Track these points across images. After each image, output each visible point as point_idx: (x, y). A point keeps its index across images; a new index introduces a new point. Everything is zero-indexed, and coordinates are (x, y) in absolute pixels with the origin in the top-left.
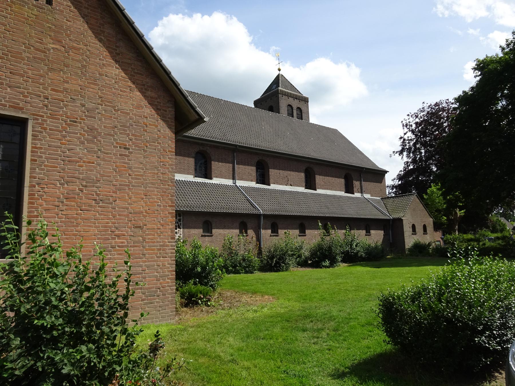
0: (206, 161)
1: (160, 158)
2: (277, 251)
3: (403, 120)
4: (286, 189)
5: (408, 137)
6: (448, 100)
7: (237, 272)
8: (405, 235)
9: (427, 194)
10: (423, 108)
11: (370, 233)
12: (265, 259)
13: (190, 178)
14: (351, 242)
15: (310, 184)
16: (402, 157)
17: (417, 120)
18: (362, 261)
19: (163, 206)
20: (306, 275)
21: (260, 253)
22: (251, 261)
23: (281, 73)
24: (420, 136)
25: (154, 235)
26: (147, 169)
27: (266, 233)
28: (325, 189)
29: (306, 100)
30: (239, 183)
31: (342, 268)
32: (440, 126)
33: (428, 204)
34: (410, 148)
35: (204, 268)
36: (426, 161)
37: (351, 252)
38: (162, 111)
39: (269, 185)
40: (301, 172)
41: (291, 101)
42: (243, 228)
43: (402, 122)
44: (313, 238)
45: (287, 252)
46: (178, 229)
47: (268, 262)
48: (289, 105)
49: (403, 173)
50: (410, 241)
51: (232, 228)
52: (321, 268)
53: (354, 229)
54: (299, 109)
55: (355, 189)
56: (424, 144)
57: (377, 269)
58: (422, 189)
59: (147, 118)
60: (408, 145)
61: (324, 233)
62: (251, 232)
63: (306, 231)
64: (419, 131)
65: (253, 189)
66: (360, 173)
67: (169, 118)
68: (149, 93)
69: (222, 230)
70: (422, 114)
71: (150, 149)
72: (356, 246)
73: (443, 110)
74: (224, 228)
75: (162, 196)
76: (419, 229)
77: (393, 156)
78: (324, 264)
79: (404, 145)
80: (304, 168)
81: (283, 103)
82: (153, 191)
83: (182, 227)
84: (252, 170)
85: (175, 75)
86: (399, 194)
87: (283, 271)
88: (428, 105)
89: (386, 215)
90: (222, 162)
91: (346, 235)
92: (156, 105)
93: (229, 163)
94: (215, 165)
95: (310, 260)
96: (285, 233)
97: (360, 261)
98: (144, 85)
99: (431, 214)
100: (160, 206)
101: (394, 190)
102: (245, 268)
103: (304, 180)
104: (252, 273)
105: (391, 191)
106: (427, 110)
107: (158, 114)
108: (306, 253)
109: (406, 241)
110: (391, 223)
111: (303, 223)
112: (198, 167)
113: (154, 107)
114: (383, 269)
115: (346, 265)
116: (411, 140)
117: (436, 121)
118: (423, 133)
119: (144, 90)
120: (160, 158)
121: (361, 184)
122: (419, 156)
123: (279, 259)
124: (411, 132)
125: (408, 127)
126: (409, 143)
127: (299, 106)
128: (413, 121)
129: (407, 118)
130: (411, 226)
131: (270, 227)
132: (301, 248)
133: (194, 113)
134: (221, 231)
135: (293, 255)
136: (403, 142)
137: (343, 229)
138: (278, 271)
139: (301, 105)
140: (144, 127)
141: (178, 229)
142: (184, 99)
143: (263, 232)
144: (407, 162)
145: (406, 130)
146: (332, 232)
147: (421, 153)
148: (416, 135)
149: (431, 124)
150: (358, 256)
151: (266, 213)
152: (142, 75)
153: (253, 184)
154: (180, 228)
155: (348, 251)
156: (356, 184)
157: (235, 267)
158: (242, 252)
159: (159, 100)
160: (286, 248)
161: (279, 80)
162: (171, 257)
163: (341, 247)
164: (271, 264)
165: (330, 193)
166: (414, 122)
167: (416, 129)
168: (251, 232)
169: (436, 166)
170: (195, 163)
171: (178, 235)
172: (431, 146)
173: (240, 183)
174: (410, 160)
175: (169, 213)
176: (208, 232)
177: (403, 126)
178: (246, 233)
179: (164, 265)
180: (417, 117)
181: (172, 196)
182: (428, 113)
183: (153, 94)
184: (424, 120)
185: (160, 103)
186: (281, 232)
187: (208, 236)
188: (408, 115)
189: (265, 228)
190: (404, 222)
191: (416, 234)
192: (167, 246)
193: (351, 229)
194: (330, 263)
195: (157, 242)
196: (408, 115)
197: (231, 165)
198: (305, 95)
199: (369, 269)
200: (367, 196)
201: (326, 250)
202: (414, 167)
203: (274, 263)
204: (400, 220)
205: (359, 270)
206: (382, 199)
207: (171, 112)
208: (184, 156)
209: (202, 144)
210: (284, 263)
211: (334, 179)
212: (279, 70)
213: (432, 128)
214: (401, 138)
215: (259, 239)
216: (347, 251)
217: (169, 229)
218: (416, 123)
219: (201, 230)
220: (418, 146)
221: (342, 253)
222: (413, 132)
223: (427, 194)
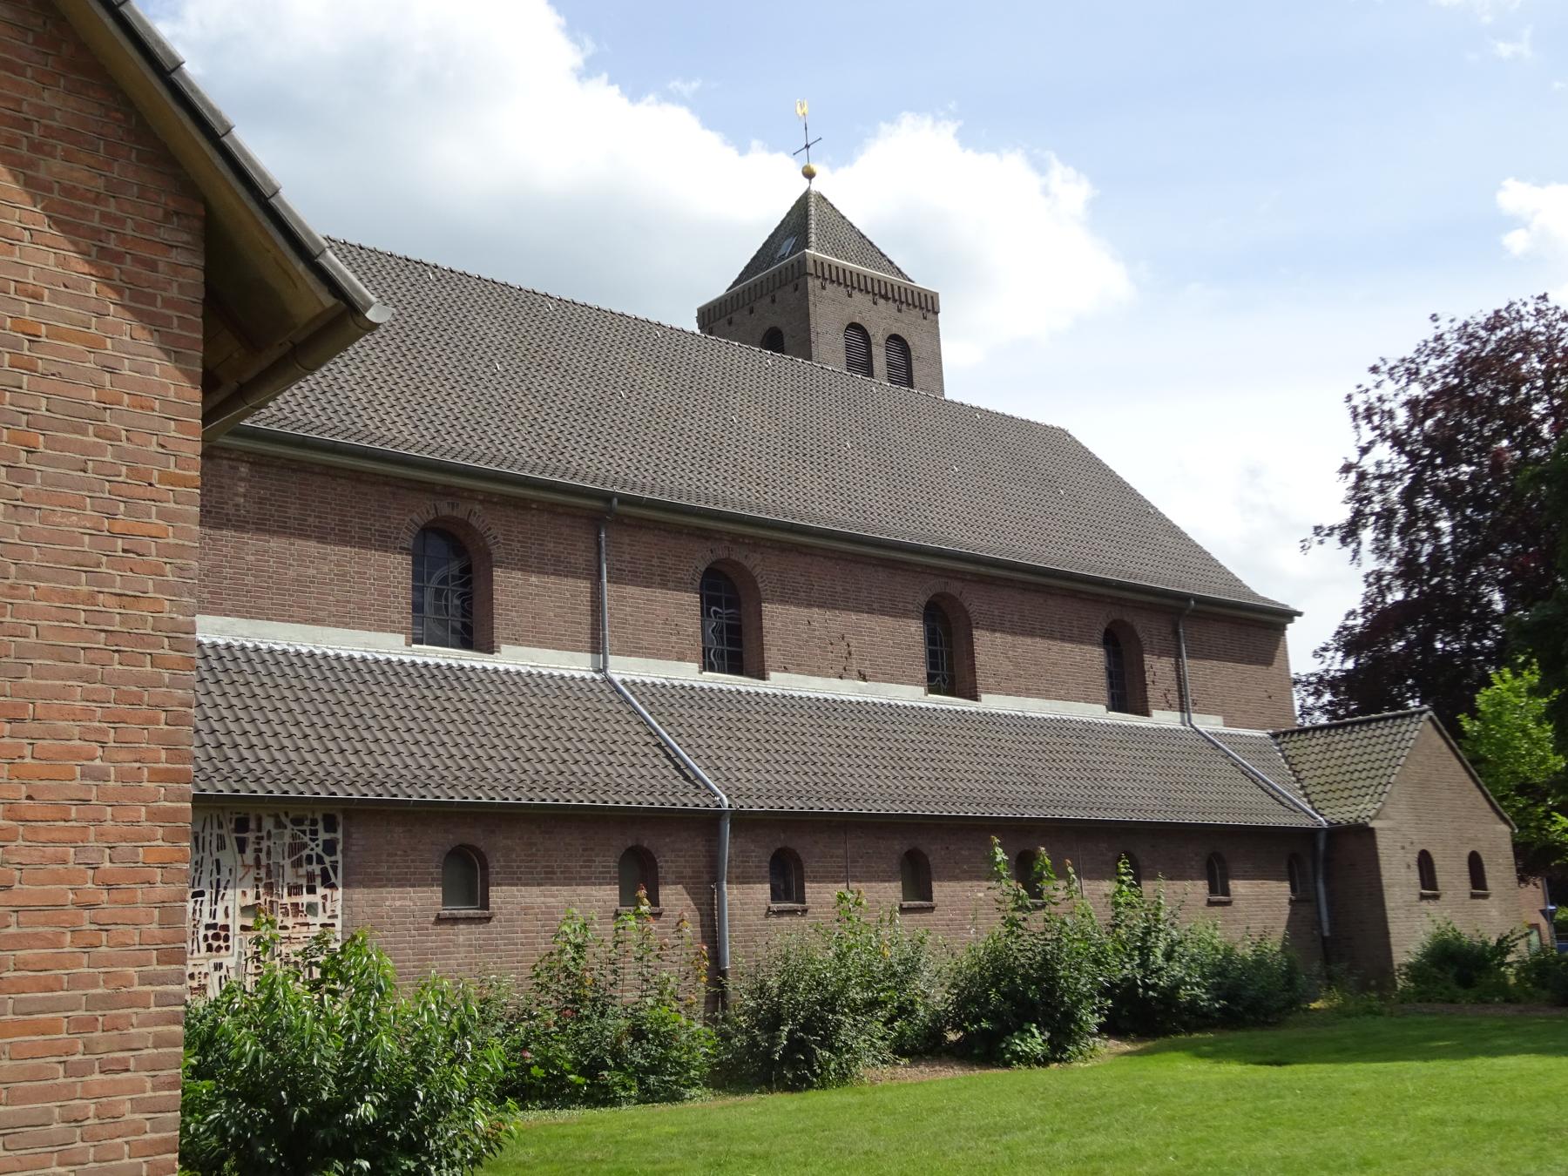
0: (467, 570)
1: (112, 516)
2: (793, 989)
3: (1353, 390)
4: (840, 698)
5: (1379, 464)
6: (1544, 298)
7: (601, 1097)
8: (1389, 904)
9: (1474, 713)
10: (1438, 338)
11: (1226, 892)
12: (739, 1029)
13: (391, 646)
14: (1143, 940)
15: (950, 670)
16: (1356, 552)
17: (1416, 390)
18: (1199, 1029)
19: (121, 777)
20: (935, 1111)
21: (718, 998)
22: (666, 1040)
23: (817, 186)
24: (1431, 457)
25: (56, 943)
26: (25, 573)
27: (746, 900)
28: (1017, 692)
29: (926, 305)
30: (623, 668)
31: (1104, 1062)
32: (1516, 416)
33: (1484, 760)
34: (1387, 515)
35: (400, 1101)
36: (1461, 570)
37: (1147, 987)
38: (128, 265)
39: (762, 676)
40: (905, 614)
41: (860, 308)
42: (639, 878)
43: (1349, 398)
44: (965, 923)
45: (841, 991)
46: (320, 891)
47: (754, 1043)
48: (854, 326)
49: (1360, 621)
50: (1411, 929)
51: (586, 881)
52: (1007, 1065)
53: (1154, 877)
54: (897, 342)
55: (1153, 693)
56: (1451, 496)
57: (1274, 1071)
58: (1450, 692)
59: (37, 296)
60: (1377, 498)
61: (1018, 897)
62: (674, 898)
63: (935, 886)
64: (1428, 440)
65: (690, 694)
66: (1168, 625)
67: (168, 303)
68: (57, 165)
69: (535, 890)
70: (1434, 363)
71: (52, 461)
72: (1168, 956)
73: (1525, 342)
74: (548, 877)
75: (116, 721)
76: (1451, 873)
77: (1315, 546)
78: (1020, 1046)
79: (1360, 501)
80: (922, 599)
81: (829, 315)
82: (64, 694)
83: (339, 881)
84: (682, 608)
85: (195, 70)
86: (1350, 714)
87: (823, 1087)
88: (1457, 325)
89: (1295, 809)
90: (541, 571)
91: (1117, 905)
92: (95, 233)
93: (573, 573)
94: (510, 588)
95: (957, 1027)
96: (842, 898)
97: (1189, 1029)
98: (26, 124)
99: (1499, 803)
100: (102, 776)
101: (1327, 697)
102: (641, 1073)
103: (920, 651)
104: (675, 1097)
105: (1310, 701)
106: (1456, 347)
107: (106, 280)
108: (933, 994)
109: (1393, 928)
110: (1322, 846)
111: (918, 849)
112: (429, 597)
113: (84, 243)
114: (1300, 1069)
115: (1127, 1047)
116: (1390, 476)
117: (1497, 393)
118: (1446, 447)
119: (24, 151)
120: (112, 516)
121: (1178, 668)
122: (1428, 548)
123: (807, 1027)
124: (1388, 444)
125: (1376, 419)
126: (1382, 490)
127: (892, 329)
128: (1396, 396)
129: (1369, 380)
130: (1413, 858)
131: (766, 869)
132: (912, 967)
133: (310, 279)
134: (533, 896)
135: (872, 1004)
136: (1357, 487)
137: (1103, 877)
138: (798, 1085)
139: (907, 325)
140: (17, 345)
141: (320, 891)
142: (253, 206)
143: (731, 894)
144: (1379, 576)
145: (1367, 434)
146: (1054, 888)
147: (1436, 534)
148: (1413, 457)
149: (1471, 405)
150: (1178, 1005)
151: (745, 804)
152: (17, 70)
153: (689, 674)
154: (333, 886)
155: (1130, 983)
156: (1158, 668)
157: (591, 1070)
158: (631, 996)
159: (112, 208)
160: (836, 972)
161: (806, 216)
162: (154, 1066)
163: (1097, 962)
164: (769, 1052)
165: (1039, 711)
166: (1403, 398)
167: (1411, 428)
168: (674, 898)
169: (1505, 586)
170: (417, 576)
171: (322, 918)
172: (1480, 503)
173: (624, 669)
174: (1390, 567)
175: (153, 815)
176: (470, 901)
177: (1355, 416)
178: (654, 901)
179: (108, 1116)
180: (1413, 375)
181: (176, 720)
182: (1461, 358)
183: (79, 175)
184: (1447, 391)
185: (121, 222)
186: (821, 894)
187: (469, 920)
188: (1374, 370)
189: (744, 879)
190: (1382, 843)
191: (1436, 897)
192: (135, 1001)
193: (1138, 878)
194: (1049, 1041)
195: (75, 982)
196: (1374, 370)
197: (584, 586)
198: (921, 282)
199: (1233, 1070)
200: (1209, 724)
201: (1026, 978)
202: (1407, 594)
203: (782, 1047)
204: (1362, 834)
205: (1185, 1075)
206: (1275, 736)
207: (181, 274)
208: (364, 543)
209: (448, 492)
210: (831, 1049)
211: (1056, 646)
212: (809, 175)
213: (1482, 424)
214: (1347, 468)
215: (712, 934)
216: (1125, 979)
217: (151, 904)
218: (1412, 404)
219: (436, 894)
220: (1422, 503)
221: (1106, 992)
222: (1398, 441)
223: (1474, 713)
